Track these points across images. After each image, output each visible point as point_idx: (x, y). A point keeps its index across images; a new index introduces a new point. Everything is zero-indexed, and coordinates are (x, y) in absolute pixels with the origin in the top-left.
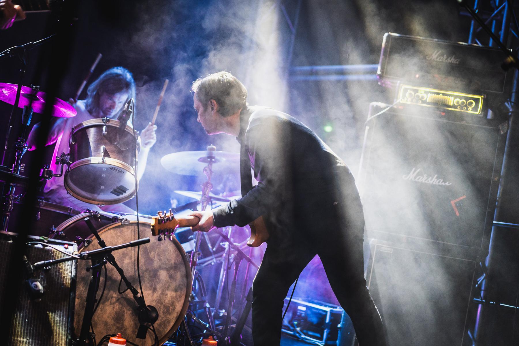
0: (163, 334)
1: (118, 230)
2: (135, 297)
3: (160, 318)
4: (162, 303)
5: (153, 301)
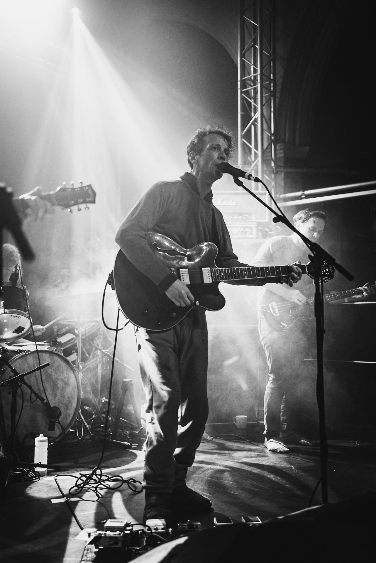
0: (67, 424)
1: (23, 359)
2: (43, 403)
3: (62, 414)
4: (62, 403)
5: (55, 403)
